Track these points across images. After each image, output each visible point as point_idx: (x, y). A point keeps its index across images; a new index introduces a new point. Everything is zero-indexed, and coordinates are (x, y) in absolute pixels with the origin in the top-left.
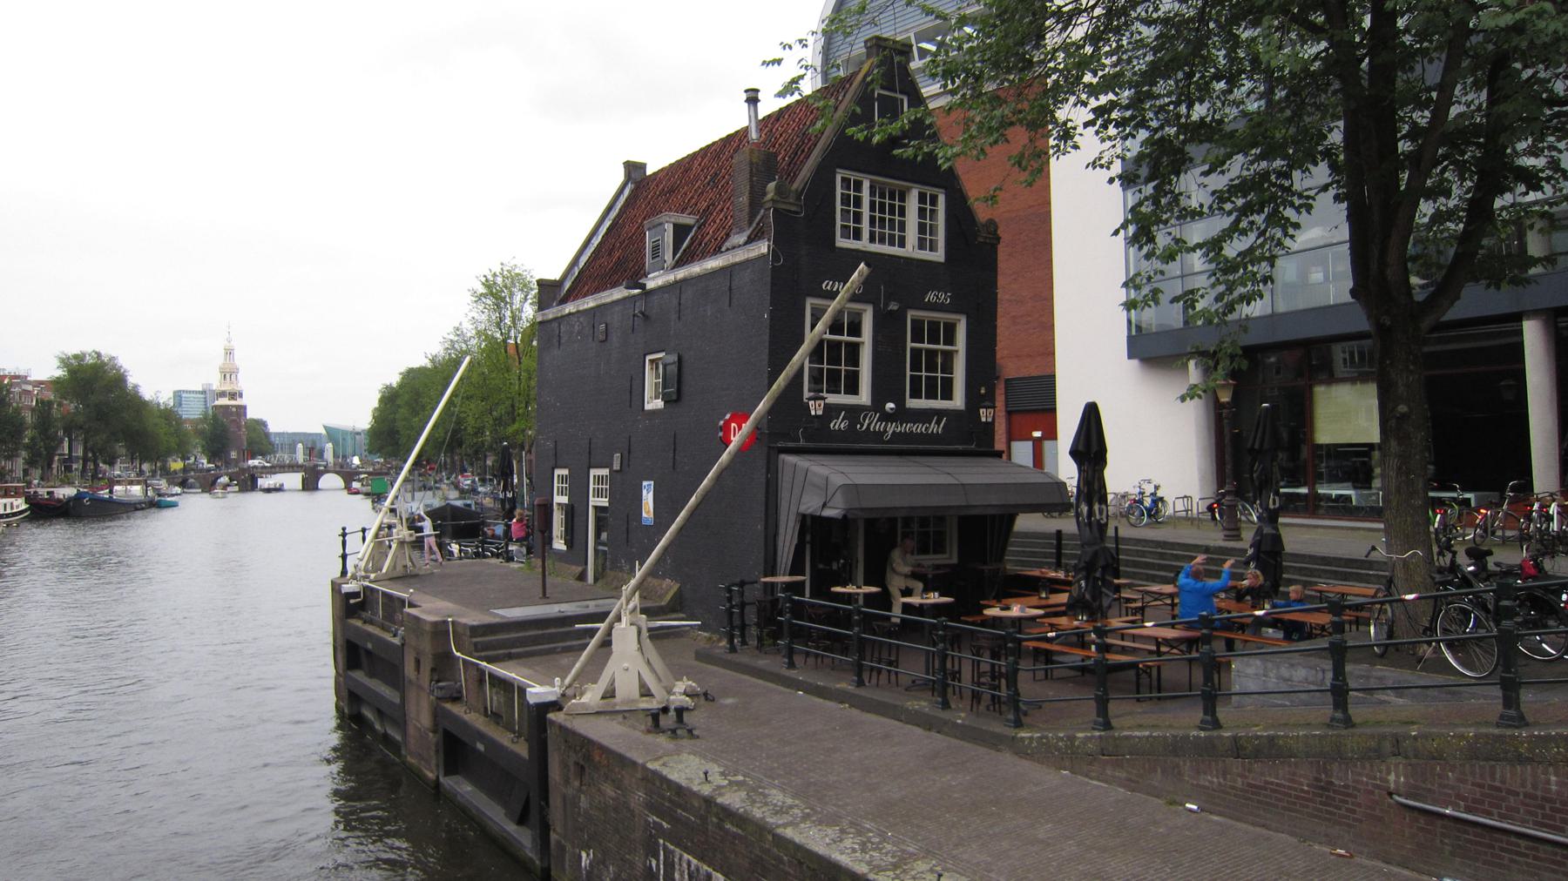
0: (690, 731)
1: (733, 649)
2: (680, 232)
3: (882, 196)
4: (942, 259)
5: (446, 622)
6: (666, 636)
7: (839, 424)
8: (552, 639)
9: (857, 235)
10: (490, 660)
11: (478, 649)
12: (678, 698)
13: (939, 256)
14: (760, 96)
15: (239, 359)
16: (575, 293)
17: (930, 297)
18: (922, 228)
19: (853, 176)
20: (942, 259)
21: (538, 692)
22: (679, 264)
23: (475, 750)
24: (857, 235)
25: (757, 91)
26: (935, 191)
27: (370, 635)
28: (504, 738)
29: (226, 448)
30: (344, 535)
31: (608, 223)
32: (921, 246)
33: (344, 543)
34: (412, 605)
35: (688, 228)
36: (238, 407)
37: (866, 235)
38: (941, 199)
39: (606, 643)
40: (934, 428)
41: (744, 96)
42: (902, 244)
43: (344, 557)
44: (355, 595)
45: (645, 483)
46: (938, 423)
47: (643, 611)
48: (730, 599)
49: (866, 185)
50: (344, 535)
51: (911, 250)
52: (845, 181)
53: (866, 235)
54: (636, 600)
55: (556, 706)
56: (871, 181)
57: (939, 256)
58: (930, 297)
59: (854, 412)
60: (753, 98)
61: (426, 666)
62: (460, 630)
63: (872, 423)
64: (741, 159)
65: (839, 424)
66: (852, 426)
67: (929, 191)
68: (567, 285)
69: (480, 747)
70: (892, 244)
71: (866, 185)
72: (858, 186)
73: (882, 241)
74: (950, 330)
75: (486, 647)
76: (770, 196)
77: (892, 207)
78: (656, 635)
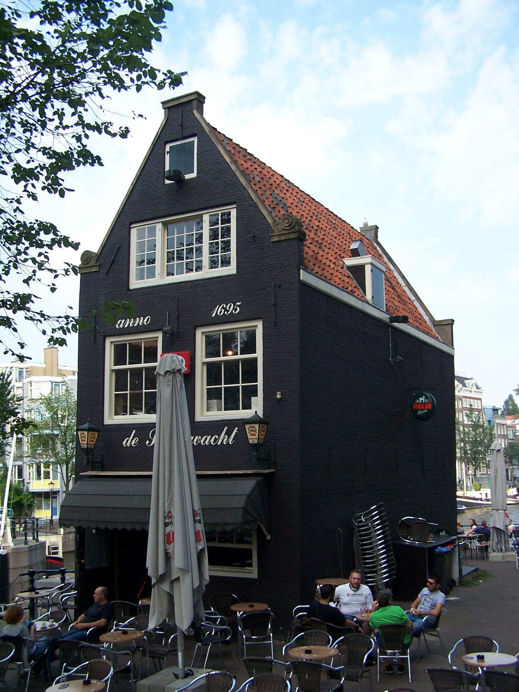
4: (234, 272)
7: (130, 441)
13: (232, 269)
17: (219, 311)
20: (234, 272)
26: (225, 209)
40: (223, 438)
46: (228, 434)
58: (219, 311)
65: (130, 441)
66: (141, 443)
67: (219, 211)
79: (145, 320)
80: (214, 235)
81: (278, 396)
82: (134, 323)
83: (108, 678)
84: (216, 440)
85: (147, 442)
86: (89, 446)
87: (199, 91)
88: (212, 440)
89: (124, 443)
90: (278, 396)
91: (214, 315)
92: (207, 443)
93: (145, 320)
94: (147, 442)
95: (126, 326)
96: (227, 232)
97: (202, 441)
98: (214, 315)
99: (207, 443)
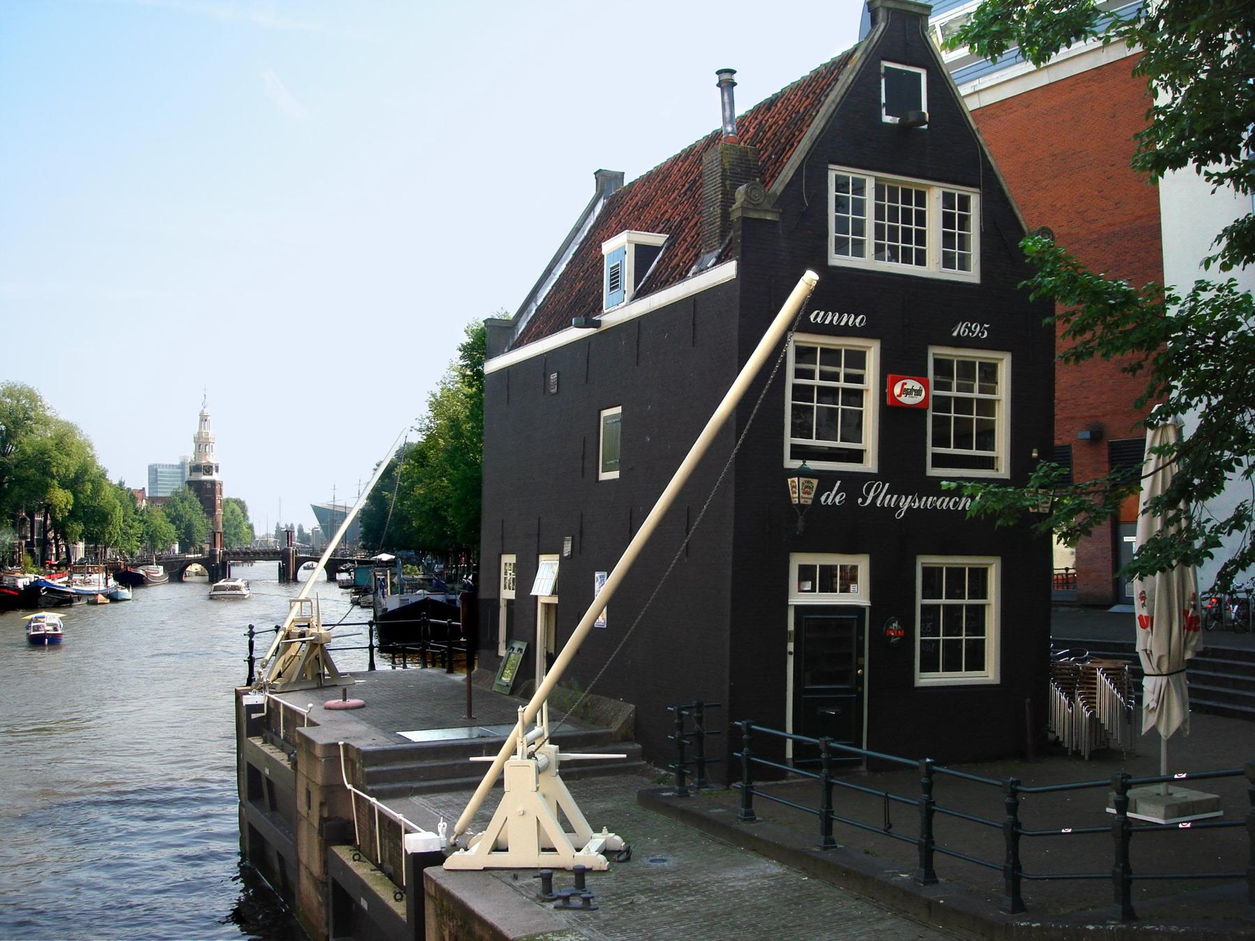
0: (587, 900)
1: (683, 794)
2: (644, 254)
3: (893, 198)
5: (337, 745)
6: (583, 774)
7: (834, 497)
8: (454, 773)
9: (859, 250)
10: (380, 796)
11: (367, 781)
12: (591, 856)
13: (973, 275)
14: (736, 78)
15: (212, 432)
16: (533, 334)
17: (960, 330)
18: (948, 239)
19: (851, 173)
21: (417, 841)
22: (640, 294)
23: (360, 907)
24: (859, 250)
25: (733, 72)
27: (269, 759)
28: (385, 892)
29: (196, 534)
30: (251, 634)
31: (574, 248)
32: (948, 262)
33: (251, 644)
34: (312, 724)
35: (654, 250)
36: (213, 483)
37: (870, 248)
38: (975, 202)
39: (499, 783)
41: (716, 79)
42: (921, 261)
43: (251, 661)
44: (258, 708)
45: (597, 575)
47: (553, 740)
48: (680, 727)
49: (870, 185)
50: (251, 634)
51: (933, 268)
52: (842, 185)
53: (870, 248)
54: (542, 728)
55: (437, 858)
56: (877, 179)
57: (973, 275)
58: (960, 330)
59: (854, 483)
60: (727, 81)
61: (316, 798)
62: (353, 755)
63: (879, 495)
64: (712, 161)
66: (851, 500)
67: (957, 190)
68: (522, 326)
69: (364, 904)
70: (907, 260)
71: (870, 185)
72: (859, 188)
73: (893, 257)
74: (989, 372)
75: (372, 778)
76: (738, 204)
77: (907, 213)
78: (568, 772)
79: (858, 320)
80: (948, 220)
81: (1035, 455)
82: (840, 320)
83: (550, 660)
84: (956, 504)
85: (860, 500)
86: (802, 501)
87: (247, 504)
88: (951, 504)
89: (823, 499)
90: (1035, 455)
91: (955, 334)
92: (829, 501)
93: (858, 320)
94: (860, 500)
95: (827, 322)
96: (964, 222)
97: (938, 503)
98: (955, 334)
99: (829, 501)
